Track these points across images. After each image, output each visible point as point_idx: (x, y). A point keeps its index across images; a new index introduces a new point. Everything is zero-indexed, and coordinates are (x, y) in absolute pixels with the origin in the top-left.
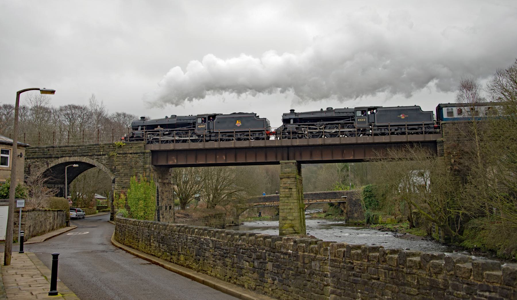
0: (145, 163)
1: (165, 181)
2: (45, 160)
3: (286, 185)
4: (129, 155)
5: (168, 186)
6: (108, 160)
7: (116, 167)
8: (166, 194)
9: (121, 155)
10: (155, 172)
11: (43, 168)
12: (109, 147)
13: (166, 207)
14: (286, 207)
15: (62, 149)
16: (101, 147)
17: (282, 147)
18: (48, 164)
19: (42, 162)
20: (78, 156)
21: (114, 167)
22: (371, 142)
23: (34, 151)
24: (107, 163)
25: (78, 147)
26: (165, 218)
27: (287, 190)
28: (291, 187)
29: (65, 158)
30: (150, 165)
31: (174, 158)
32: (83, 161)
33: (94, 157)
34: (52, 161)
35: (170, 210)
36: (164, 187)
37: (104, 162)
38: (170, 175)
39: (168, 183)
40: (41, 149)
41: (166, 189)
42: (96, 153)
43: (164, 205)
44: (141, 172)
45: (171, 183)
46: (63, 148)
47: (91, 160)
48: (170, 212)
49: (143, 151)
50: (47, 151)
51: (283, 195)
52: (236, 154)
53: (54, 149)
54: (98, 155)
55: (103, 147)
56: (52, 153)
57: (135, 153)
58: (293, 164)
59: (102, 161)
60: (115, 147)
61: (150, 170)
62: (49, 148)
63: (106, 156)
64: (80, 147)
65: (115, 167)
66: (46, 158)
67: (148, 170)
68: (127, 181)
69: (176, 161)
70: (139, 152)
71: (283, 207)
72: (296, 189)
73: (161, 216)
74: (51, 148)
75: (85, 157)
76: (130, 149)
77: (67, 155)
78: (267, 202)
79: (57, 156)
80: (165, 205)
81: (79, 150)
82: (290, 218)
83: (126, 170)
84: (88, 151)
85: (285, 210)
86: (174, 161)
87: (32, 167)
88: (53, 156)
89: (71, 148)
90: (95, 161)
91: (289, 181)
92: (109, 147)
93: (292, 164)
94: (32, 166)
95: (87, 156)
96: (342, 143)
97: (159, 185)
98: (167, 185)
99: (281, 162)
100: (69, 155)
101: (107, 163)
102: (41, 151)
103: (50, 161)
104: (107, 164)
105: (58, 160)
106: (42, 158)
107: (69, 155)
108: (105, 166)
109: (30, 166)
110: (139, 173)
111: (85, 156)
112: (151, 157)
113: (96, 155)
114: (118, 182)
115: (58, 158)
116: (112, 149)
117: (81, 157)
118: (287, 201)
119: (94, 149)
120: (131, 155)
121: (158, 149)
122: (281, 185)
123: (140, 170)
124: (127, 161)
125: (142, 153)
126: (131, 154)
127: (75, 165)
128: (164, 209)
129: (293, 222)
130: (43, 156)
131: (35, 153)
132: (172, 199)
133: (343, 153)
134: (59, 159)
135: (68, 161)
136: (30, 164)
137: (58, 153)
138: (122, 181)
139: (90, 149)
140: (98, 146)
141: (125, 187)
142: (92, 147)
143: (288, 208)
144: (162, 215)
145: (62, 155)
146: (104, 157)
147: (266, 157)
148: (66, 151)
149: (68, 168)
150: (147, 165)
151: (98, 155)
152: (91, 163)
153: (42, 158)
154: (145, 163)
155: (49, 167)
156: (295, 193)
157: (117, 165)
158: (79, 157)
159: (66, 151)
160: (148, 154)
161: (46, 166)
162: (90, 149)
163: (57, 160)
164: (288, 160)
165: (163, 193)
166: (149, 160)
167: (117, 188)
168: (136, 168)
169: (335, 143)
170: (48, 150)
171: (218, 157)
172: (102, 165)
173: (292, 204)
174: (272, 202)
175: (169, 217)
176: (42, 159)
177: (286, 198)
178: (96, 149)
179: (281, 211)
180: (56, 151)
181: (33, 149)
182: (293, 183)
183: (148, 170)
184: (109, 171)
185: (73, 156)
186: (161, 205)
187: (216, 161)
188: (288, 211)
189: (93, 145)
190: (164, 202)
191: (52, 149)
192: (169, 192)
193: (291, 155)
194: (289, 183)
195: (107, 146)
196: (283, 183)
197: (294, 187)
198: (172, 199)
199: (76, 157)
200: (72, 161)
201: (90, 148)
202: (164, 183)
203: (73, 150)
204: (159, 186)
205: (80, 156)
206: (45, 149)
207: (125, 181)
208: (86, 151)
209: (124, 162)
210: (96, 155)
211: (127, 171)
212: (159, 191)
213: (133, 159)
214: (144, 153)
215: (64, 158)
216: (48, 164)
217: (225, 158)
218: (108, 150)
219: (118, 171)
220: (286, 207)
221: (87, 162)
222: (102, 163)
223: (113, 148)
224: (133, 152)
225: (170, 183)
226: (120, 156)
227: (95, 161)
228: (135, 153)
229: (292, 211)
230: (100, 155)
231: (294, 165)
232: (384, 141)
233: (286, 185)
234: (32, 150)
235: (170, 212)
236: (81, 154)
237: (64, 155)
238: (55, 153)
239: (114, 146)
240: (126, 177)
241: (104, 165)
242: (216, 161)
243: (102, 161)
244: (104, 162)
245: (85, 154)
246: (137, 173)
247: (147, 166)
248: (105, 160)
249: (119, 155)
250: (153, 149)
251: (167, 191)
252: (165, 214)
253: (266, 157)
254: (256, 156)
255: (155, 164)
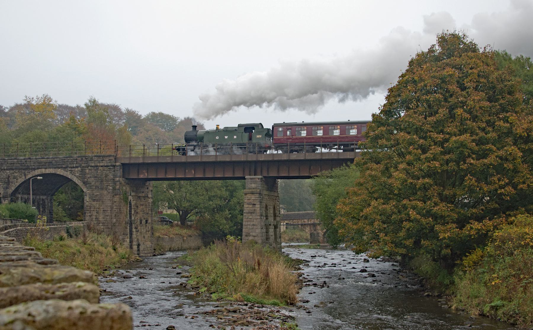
0: (115, 176)
1: (140, 195)
2: (23, 171)
3: (250, 201)
4: (100, 168)
5: (145, 199)
6: (81, 172)
7: (88, 179)
8: (141, 208)
9: (93, 168)
10: (127, 185)
11: (21, 179)
12: (82, 159)
13: (141, 221)
14: (249, 223)
15: (39, 161)
16: (74, 159)
17: (250, 162)
18: (25, 175)
19: (20, 173)
20: (53, 168)
21: (86, 179)
22: (335, 158)
23: (12, 162)
24: (79, 175)
25: (53, 159)
26: (139, 231)
27: (251, 206)
28: (255, 203)
29: (41, 169)
30: (121, 179)
31: (144, 171)
32: (58, 173)
33: (68, 169)
34: (29, 173)
35: (147, 224)
36: (140, 201)
37: (77, 174)
38: (148, 188)
39: (144, 197)
40: (20, 160)
41: (142, 203)
42: (69, 166)
43: (139, 218)
44: (111, 185)
45: (149, 196)
46: (40, 160)
47: (65, 172)
48: (146, 226)
49: (114, 164)
50: (25, 163)
51: (247, 211)
52: (234, 169)
53: (31, 160)
54: (71, 168)
55: (76, 159)
56: (29, 165)
57: (106, 166)
58: (259, 179)
59: (75, 174)
60: (87, 160)
61: (121, 183)
62: (26, 160)
63: (79, 169)
64: (55, 159)
65: (87, 180)
66: (24, 169)
67: (118, 183)
68: (98, 193)
69: (146, 174)
70: (109, 165)
71: (246, 223)
72: (259, 206)
73: (134, 230)
74: (28, 160)
75: (60, 169)
76: (101, 162)
77: (43, 167)
78: (286, 220)
79: (33, 167)
80: (140, 218)
81: (54, 162)
82: (254, 234)
83: (97, 183)
84: (62, 163)
85: (248, 226)
86: (145, 175)
87: (11, 178)
88: (31, 167)
89: (47, 160)
90: (69, 173)
91: (253, 197)
92: (82, 159)
93: (257, 179)
94: (11, 177)
95: (61, 168)
96: (306, 158)
97: (133, 198)
98: (143, 199)
99: (246, 177)
100: (45, 167)
101: (79, 175)
102: (19, 162)
103: (27, 173)
104: (80, 177)
105: (35, 172)
106: (20, 169)
107: (45, 167)
108: (78, 178)
109: (9, 177)
110: (110, 186)
111: (59, 168)
112: (121, 170)
113: (70, 167)
114: (89, 194)
115: (34, 169)
116: (85, 162)
117: (56, 169)
118: (251, 217)
119: (67, 162)
120: (101, 168)
121: (229, 160)
122: (246, 201)
123: (110, 182)
124: (98, 173)
125: (112, 166)
126: (102, 166)
127: (39, 178)
128: (139, 223)
129: (256, 238)
130: (21, 167)
131: (14, 164)
132: (150, 213)
133: (204, 170)
134: (36, 171)
135: (44, 173)
136: (9, 175)
137: (34, 164)
138: (93, 194)
139: (64, 161)
140: (71, 159)
141: (97, 199)
142: (66, 159)
143: (251, 224)
144: (136, 228)
145: (38, 167)
146: (77, 169)
147: (204, 173)
148: (42, 163)
149: (32, 180)
150: (117, 178)
151: (71, 168)
152: (65, 175)
153: (20, 169)
154: (115, 176)
155: (27, 178)
156: (259, 209)
157: (89, 178)
158: (54, 169)
159: (42, 163)
160: (118, 167)
161: (24, 177)
162: (64, 161)
163: (33, 172)
164: (250, 175)
165: (137, 207)
166: (119, 173)
167: (88, 201)
168: (107, 181)
169: (299, 159)
170: (26, 161)
171: (187, 171)
172: (75, 177)
173: (255, 221)
174: (292, 221)
175: (145, 231)
176: (20, 170)
177: (249, 214)
178: (70, 161)
179: (244, 227)
180: (33, 162)
181: (12, 160)
182: (257, 199)
183: (118, 183)
184: (82, 183)
185: (49, 168)
186: (135, 218)
187: (185, 175)
188: (251, 227)
189: (67, 157)
190: (138, 215)
191: (29, 160)
192: (146, 205)
193: (259, 170)
194: (253, 198)
195: (80, 159)
196: (247, 199)
197: (258, 203)
198: (150, 213)
199: (52, 169)
200: (48, 173)
201: (64, 160)
202: (139, 197)
203: (49, 161)
204: (132, 200)
205: (55, 168)
206: (23, 161)
207: (96, 194)
208: (60, 163)
209: (95, 175)
210: (70, 167)
211: (98, 184)
212: (132, 204)
213: (104, 172)
214: (114, 166)
215: (40, 170)
216: (25, 175)
217: (193, 173)
218: (81, 163)
219: (90, 184)
220: (249, 223)
221: (62, 174)
222: (75, 176)
223: (85, 160)
224: (103, 165)
225: (147, 197)
226: (92, 169)
227: (69, 173)
228: (106, 166)
229: (255, 227)
230: (74, 167)
231: (259, 180)
232: (348, 157)
233: (250, 201)
234: (11, 161)
235: (146, 226)
236: (55, 166)
237: (40, 167)
238: (32, 164)
239: (86, 159)
240: (97, 190)
241: (77, 177)
242: (185, 175)
243: (75, 174)
244: (77, 174)
245: (60, 166)
246: (107, 186)
247: (117, 179)
248: (78, 172)
249: (91, 168)
250: (123, 162)
251: (143, 205)
252: (139, 228)
253: (204, 173)
254: (175, 173)
255: (127, 177)
